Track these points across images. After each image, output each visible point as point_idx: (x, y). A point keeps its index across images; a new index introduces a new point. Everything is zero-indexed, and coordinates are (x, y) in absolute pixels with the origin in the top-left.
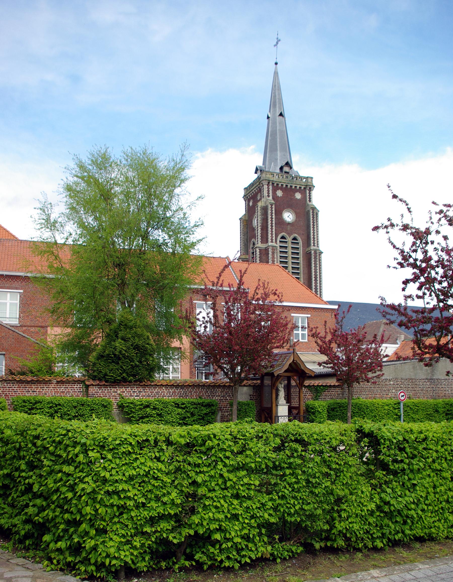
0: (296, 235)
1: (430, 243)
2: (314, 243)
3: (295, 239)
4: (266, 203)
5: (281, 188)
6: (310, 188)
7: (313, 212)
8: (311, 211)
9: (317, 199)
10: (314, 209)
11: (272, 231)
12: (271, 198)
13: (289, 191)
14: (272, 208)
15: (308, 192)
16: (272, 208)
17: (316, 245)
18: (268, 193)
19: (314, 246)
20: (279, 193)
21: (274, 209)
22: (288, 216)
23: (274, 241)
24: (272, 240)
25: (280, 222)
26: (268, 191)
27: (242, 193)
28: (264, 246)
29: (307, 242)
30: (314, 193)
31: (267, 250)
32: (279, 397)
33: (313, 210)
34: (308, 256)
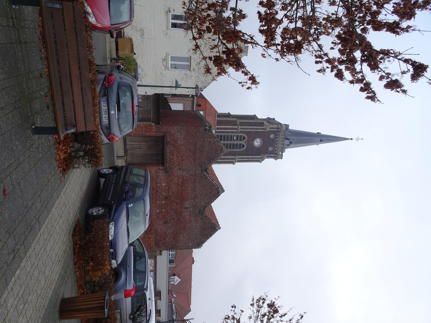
0: (246, 146)
1: (264, 53)
2: (240, 158)
3: (243, 146)
4: (266, 125)
5: (275, 138)
6: (275, 157)
7: (260, 158)
8: (261, 157)
9: (269, 162)
10: (263, 159)
11: (251, 129)
12: (270, 129)
13: (273, 142)
14: (263, 129)
15: (273, 155)
16: (263, 129)
17: (239, 159)
18: (272, 128)
19: (239, 158)
20: (272, 136)
21: (274, 130)
22: (257, 143)
23: (239, 159)
24: (242, 129)
25: (252, 136)
26: (274, 128)
27: (271, 117)
28: (238, 123)
29: (240, 154)
30: (272, 160)
31: (236, 125)
32: (134, 100)
33: (262, 158)
34: (234, 154)
